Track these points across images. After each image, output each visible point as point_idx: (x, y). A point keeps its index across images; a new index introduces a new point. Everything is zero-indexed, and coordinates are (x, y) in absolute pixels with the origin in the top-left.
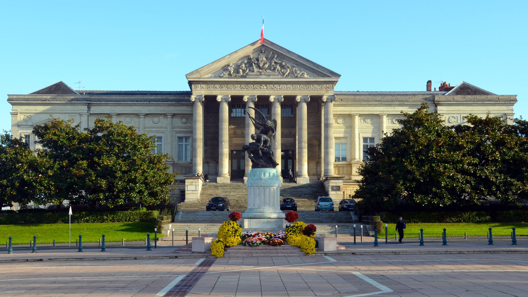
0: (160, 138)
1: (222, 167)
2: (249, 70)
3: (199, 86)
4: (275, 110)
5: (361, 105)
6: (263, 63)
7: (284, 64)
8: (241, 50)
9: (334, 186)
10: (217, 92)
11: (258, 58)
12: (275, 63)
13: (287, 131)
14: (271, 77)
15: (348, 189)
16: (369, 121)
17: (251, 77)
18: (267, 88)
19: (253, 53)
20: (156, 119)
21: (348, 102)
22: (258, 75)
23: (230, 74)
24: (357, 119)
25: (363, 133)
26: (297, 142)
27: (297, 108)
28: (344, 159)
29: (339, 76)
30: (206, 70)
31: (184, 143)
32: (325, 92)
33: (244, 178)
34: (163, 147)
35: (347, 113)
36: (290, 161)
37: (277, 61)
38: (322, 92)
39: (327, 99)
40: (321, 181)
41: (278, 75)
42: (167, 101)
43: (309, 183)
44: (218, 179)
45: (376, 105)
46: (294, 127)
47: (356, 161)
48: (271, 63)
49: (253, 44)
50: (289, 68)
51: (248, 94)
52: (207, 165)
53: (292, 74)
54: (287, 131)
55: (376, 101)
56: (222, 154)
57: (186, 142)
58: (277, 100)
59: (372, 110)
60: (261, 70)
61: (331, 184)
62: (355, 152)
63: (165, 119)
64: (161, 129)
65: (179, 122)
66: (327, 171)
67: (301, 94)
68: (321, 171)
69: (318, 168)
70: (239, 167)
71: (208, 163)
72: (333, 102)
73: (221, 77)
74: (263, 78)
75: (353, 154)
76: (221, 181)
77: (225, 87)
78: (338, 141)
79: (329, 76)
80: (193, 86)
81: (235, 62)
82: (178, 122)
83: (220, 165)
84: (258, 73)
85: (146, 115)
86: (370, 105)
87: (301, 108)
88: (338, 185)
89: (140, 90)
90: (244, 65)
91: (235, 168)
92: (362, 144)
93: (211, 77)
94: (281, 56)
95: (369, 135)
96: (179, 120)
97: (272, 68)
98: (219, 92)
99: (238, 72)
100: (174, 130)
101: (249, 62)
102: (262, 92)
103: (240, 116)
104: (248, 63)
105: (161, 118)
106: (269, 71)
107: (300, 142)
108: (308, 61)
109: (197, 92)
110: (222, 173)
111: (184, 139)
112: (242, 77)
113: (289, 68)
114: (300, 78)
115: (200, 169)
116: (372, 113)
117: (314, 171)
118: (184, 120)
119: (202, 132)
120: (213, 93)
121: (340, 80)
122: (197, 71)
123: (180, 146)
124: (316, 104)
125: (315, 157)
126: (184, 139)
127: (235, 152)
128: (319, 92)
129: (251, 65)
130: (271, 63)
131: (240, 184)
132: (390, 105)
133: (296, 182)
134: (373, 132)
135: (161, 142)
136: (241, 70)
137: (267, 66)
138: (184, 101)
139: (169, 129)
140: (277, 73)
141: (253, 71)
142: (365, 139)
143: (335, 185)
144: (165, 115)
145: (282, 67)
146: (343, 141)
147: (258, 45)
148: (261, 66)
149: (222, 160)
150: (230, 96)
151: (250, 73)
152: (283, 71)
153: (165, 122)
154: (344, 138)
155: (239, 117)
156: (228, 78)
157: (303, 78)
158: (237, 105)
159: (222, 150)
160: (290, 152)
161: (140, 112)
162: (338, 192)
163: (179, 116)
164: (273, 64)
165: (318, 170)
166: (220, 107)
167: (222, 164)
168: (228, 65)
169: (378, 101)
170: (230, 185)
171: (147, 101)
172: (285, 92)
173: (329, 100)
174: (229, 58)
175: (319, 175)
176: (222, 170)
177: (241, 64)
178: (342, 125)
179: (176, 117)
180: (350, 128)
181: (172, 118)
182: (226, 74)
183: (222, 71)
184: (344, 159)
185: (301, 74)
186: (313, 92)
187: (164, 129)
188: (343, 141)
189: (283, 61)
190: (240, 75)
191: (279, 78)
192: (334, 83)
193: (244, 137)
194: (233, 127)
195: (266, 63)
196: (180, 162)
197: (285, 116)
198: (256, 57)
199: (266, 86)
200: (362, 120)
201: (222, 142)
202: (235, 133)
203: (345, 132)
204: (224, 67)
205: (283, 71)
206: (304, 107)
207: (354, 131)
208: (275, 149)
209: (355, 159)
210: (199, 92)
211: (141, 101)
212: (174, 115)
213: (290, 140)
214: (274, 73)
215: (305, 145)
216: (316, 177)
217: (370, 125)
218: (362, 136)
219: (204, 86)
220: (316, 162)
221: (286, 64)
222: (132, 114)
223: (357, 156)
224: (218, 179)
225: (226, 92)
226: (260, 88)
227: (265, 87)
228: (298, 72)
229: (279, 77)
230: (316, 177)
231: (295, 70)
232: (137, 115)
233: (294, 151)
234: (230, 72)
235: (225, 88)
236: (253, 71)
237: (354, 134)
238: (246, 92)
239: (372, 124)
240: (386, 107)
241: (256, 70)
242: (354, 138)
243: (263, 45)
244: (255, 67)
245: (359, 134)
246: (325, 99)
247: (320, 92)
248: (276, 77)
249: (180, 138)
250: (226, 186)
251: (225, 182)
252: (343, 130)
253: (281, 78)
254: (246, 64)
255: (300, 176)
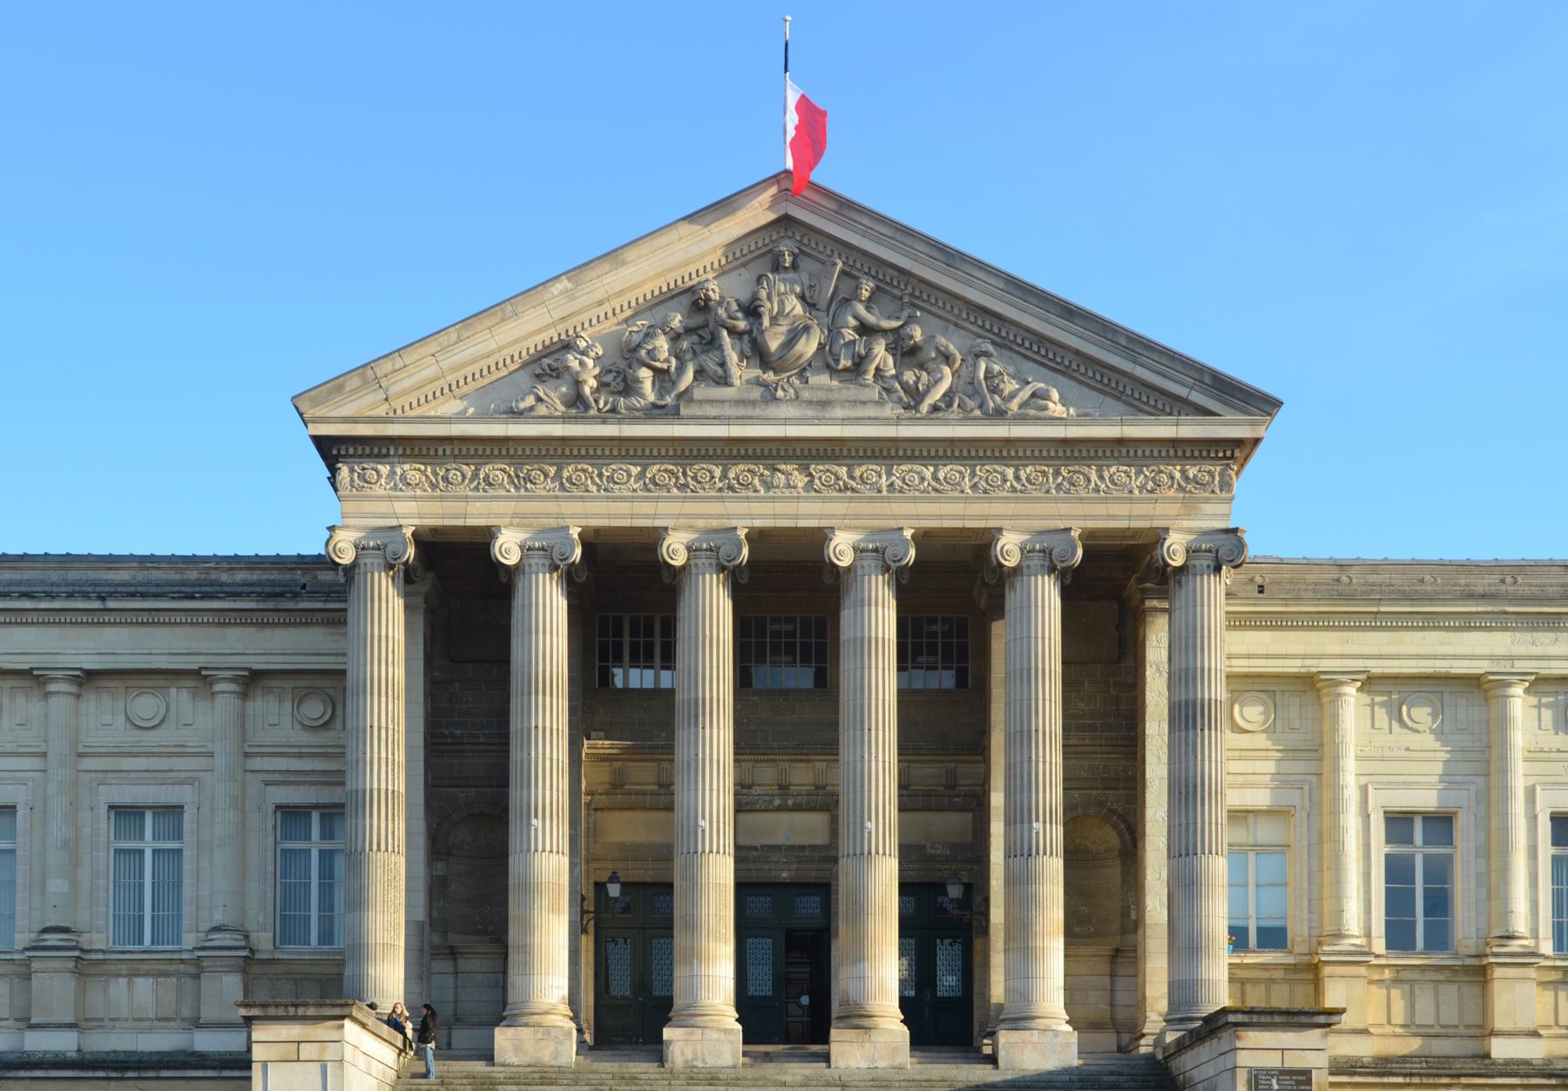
0: (171, 813)
1: (527, 968)
2: (700, 373)
3: (384, 469)
4: (860, 622)
5: (1377, 622)
6: (784, 328)
7: (917, 334)
8: (644, 248)
9: (1269, 1072)
10: (497, 506)
11: (755, 297)
12: (865, 329)
13: (930, 772)
14: (839, 412)
16: (1421, 714)
17: (711, 411)
18: (809, 486)
19: (722, 273)
20: (146, 705)
21: (1298, 599)
22: (753, 403)
23: (577, 401)
24: (1352, 706)
25: (1390, 786)
26: (997, 828)
27: (997, 628)
28: (1273, 937)
29: (1265, 405)
30: (423, 369)
31: (315, 844)
32: (1175, 508)
34: (187, 866)
35: (1292, 666)
36: (947, 955)
37: (871, 319)
38: (1161, 509)
39: (1191, 552)
40: (1150, 1057)
41: (880, 403)
42: (206, 596)
43: (1076, 1062)
44: (503, 1038)
45: (1467, 623)
46: (979, 747)
47: (1345, 945)
48: (833, 332)
49: (724, 207)
50: (947, 358)
51: (687, 521)
52: (445, 965)
53: (973, 396)
54: (930, 772)
55: (1471, 596)
56: (527, 888)
57: (327, 834)
58: (876, 554)
59: (1440, 650)
60: (770, 376)
61: (1245, 1059)
62: (1338, 898)
63: (203, 706)
64: (177, 763)
65: (287, 720)
66: (1183, 991)
67: (1022, 520)
68: (1140, 1003)
69: (1121, 983)
70: (642, 985)
71: (453, 953)
72: (1227, 575)
73: (515, 414)
74: (786, 421)
75: (1328, 906)
76: (517, 1049)
77: (543, 479)
78: (1240, 835)
79: (1205, 412)
80: (344, 471)
81: (609, 326)
82: (275, 718)
83: (513, 957)
84: (757, 393)
85: (88, 678)
86: (1431, 622)
87: (1027, 607)
88: (1294, 1061)
90: (662, 344)
91: (621, 986)
92: (1380, 849)
93: (460, 418)
94: (899, 288)
95: (1426, 799)
96: (288, 705)
97: (845, 362)
98: (509, 507)
99: (629, 387)
100: (257, 763)
101: (699, 321)
102: (780, 508)
104: (689, 331)
106: (822, 379)
107: (1019, 815)
108: (1069, 312)
109: (368, 507)
110: (526, 1000)
111: (315, 818)
112: (656, 412)
113: (947, 358)
114: (1021, 419)
115: (389, 977)
116: (1441, 667)
117: (1097, 1005)
119: (401, 757)
121: (1275, 434)
122: (366, 373)
123: (290, 861)
124: (1116, 587)
125: (1104, 923)
126: (315, 818)
128: (1137, 509)
129: (713, 343)
130: (833, 332)
131: (642, 1068)
133: (993, 1060)
134: (1449, 779)
135: (178, 836)
136: (645, 374)
137: (808, 347)
138: (314, 594)
139: (220, 762)
140: (875, 393)
141: (724, 381)
142: (1399, 823)
143: (1272, 1061)
144: (199, 678)
145: (907, 353)
146: (1266, 832)
147: (757, 213)
148: (774, 345)
149: (527, 926)
150: (575, 532)
151: (700, 392)
152: (909, 377)
153: (203, 720)
154: (1270, 813)
155: (642, 692)
156: (565, 419)
157: (1037, 420)
158: (634, 647)
159: (528, 866)
161: (47, 661)
163: (288, 684)
164: (849, 334)
165: (1121, 998)
166: (518, 602)
167: (526, 949)
168: (567, 346)
169: (1483, 597)
170: (576, 1077)
171: (86, 596)
172: (923, 508)
173: (1204, 562)
174: (569, 295)
175: (1132, 1028)
177: (649, 335)
178: (1261, 741)
179: (269, 690)
180: (1312, 755)
181: (244, 696)
182: (554, 395)
183: (524, 379)
184: (1273, 937)
185: (1025, 394)
186: (1100, 509)
187: (193, 763)
188: (1266, 832)
189: (911, 319)
190: (635, 402)
191: (886, 421)
192: (1235, 451)
193: (670, 808)
194: (604, 745)
195: (807, 329)
196: (289, 952)
197: (919, 685)
198: (745, 296)
199: (805, 469)
200: (1381, 713)
201: (526, 816)
202: (617, 785)
203: (1281, 781)
204: (536, 359)
205: (909, 377)
206: (1046, 602)
207: (1336, 770)
208: (862, 855)
209: (1339, 935)
210: (383, 507)
211: (51, 596)
212: (253, 681)
213: (952, 823)
214: (852, 392)
215: (1050, 833)
216: (1107, 1040)
217: (1429, 741)
218: (1383, 800)
219: (412, 471)
220: (1106, 950)
221: (930, 338)
223: (1353, 922)
224: (503, 1038)
225: (551, 507)
226: (768, 486)
227: (800, 480)
228: (1010, 386)
229: (888, 411)
230: (1107, 1040)
231: (989, 375)
233: (977, 892)
234: (578, 384)
235: (545, 486)
236: (724, 381)
237: (1337, 788)
238: (674, 508)
239: (1439, 734)
240: (1527, 636)
241: (741, 372)
242: (1336, 811)
243: (785, 222)
244: (733, 357)
245: (1364, 790)
246: (1175, 550)
247: (1146, 509)
248: (870, 411)
249: (292, 816)
251: (546, 1055)
252: (1270, 767)
253: (898, 421)
254: (675, 338)
255: (1020, 1021)
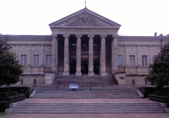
13: (95, 52)
14: (89, 26)
15: (38, 78)
17: (79, 26)
20: (36, 47)
29: (120, 25)
32: (114, 33)
33: (76, 73)
34: (39, 59)
36: (97, 66)
51: (79, 34)
71: (59, 66)
82: (47, 48)
88: (123, 76)
89: (126, 36)
100: (45, 51)
103: (74, 45)
105: (39, 46)
116: (133, 44)
118: (49, 47)
120: (62, 33)
121: (121, 27)
127: (72, 62)
132: (142, 41)
133: (100, 75)
139: (42, 51)
143: (121, 76)
153: (41, 48)
160: (97, 62)
162: (123, 80)
176: (100, 68)
212: (45, 45)
222: (26, 44)
232: (28, 45)
249: (47, 55)
250: (67, 77)
